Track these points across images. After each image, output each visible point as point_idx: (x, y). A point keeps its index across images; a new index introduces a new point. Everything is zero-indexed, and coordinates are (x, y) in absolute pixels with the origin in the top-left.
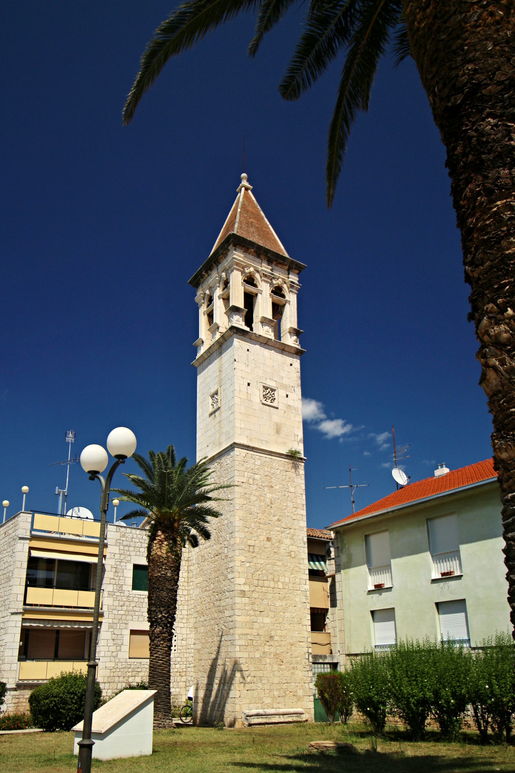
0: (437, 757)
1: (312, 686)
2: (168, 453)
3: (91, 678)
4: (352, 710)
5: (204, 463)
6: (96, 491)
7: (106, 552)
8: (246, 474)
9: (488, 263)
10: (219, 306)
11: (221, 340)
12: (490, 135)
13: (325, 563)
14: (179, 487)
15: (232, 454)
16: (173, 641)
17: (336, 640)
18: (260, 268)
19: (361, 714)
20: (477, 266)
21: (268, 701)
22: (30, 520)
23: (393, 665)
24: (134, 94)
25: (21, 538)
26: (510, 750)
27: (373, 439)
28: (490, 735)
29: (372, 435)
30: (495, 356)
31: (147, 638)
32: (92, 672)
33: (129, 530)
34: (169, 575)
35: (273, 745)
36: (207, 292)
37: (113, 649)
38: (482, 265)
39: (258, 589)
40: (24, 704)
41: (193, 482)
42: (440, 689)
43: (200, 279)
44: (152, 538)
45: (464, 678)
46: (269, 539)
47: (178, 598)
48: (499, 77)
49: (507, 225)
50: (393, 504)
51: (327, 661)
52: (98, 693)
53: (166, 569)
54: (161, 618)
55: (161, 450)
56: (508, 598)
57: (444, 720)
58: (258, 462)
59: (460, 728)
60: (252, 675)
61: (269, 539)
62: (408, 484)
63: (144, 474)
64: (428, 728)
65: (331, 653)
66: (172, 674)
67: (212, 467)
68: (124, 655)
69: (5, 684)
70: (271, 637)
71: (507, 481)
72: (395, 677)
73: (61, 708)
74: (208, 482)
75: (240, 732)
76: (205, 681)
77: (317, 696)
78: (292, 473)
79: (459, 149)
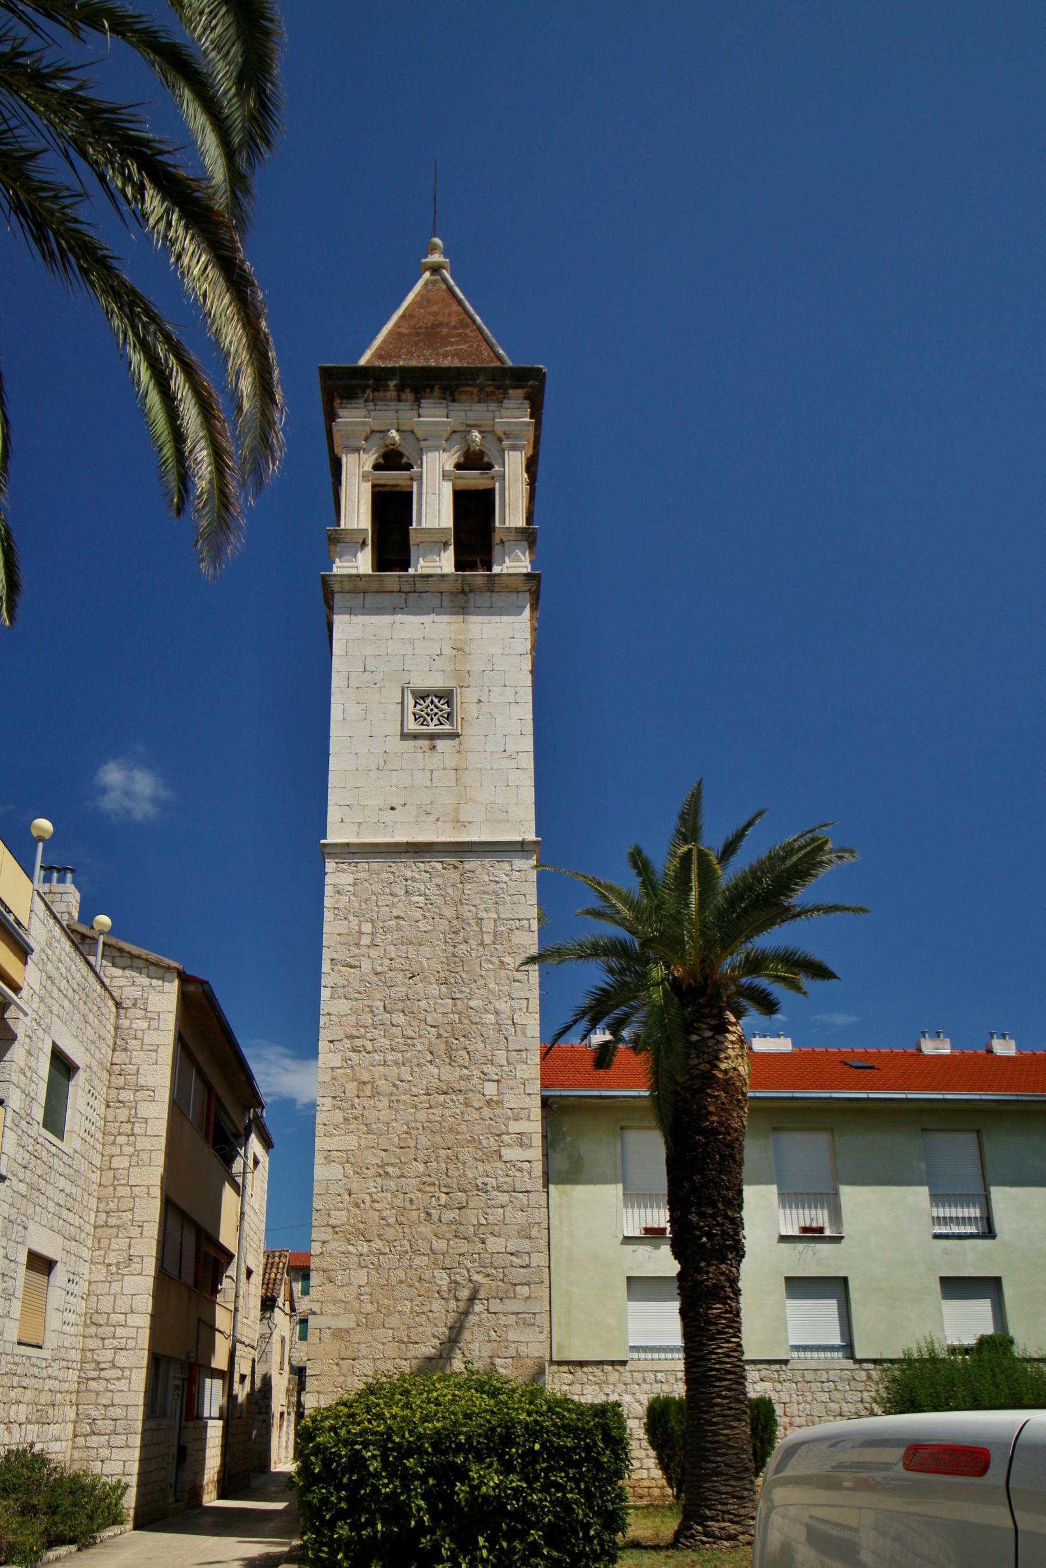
43: (368, 386)
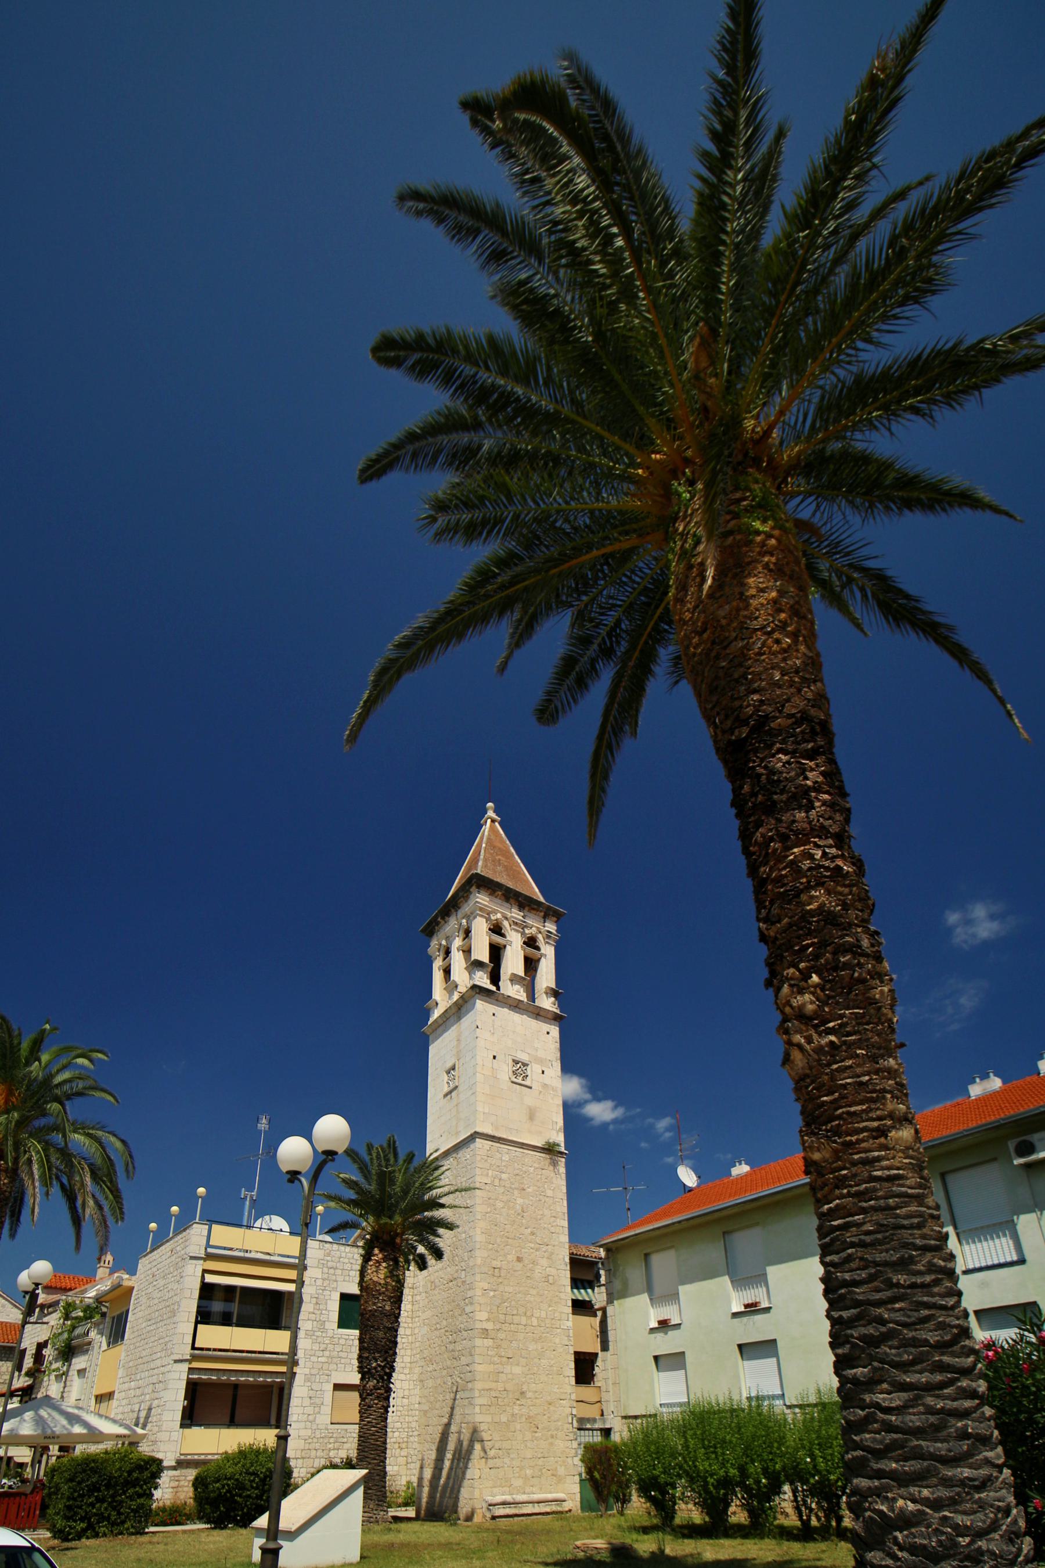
0: (746, 1560)
1: (577, 1460)
2: (389, 1145)
3: (280, 1454)
4: (630, 1495)
5: (437, 1159)
6: (294, 1197)
7: (307, 1275)
8: (490, 1172)
9: (786, 920)
10: (458, 960)
11: (461, 1001)
12: (781, 773)
13: (593, 1290)
14: (403, 1191)
15: (472, 1146)
16: (391, 1399)
17: (608, 1397)
18: (509, 915)
19: (643, 1500)
20: (773, 923)
21: (518, 1483)
22: (206, 1233)
23: (685, 1432)
24: (360, 714)
25: (192, 1258)
26: (841, 1548)
27: (652, 1126)
28: (815, 1528)
29: (650, 1120)
30: (800, 1032)
31: (355, 1396)
32: (283, 1446)
33: (335, 1246)
34: (387, 1308)
35: (524, 1547)
36: (444, 942)
37: (309, 1410)
38: (779, 921)
39: (505, 1327)
40: (185, 1489)
41: (422, 1184)
42: (746, 1463)
44: (367, 1258)
45: (779, 1448)
46: (519, 1259)
47: (399, 1339)
48: (788, 709)
49: (807, 877)
50: (680, 1211)
51: (596, 1426)
52: (288, 1473)
53: (383, 1300)
54: (375, 1368)
55: (380, 1142)
56: (830, 1343)
57: (753, 1507)
58: (506, 1158)
59: (775, 1518)
60: (497, 1446)
61: (519, 1259)
62: (698, 1186)
63: (357, 1172)
64: (733, 1519)
65: (602, 1415)
66: (388, 1446)
67: (446, 1164)
68: (324, 1419)
69: (161, 1461)
70: (522, 1393)
71: (822, 1189)
72: (688, 1447)
73: (236, 1495)
74: (441, 1183)
75: (480, 1529)
76: (433, 1455)
77: (584, 1475)
78: (549, 1172)
79: (746, 788)
